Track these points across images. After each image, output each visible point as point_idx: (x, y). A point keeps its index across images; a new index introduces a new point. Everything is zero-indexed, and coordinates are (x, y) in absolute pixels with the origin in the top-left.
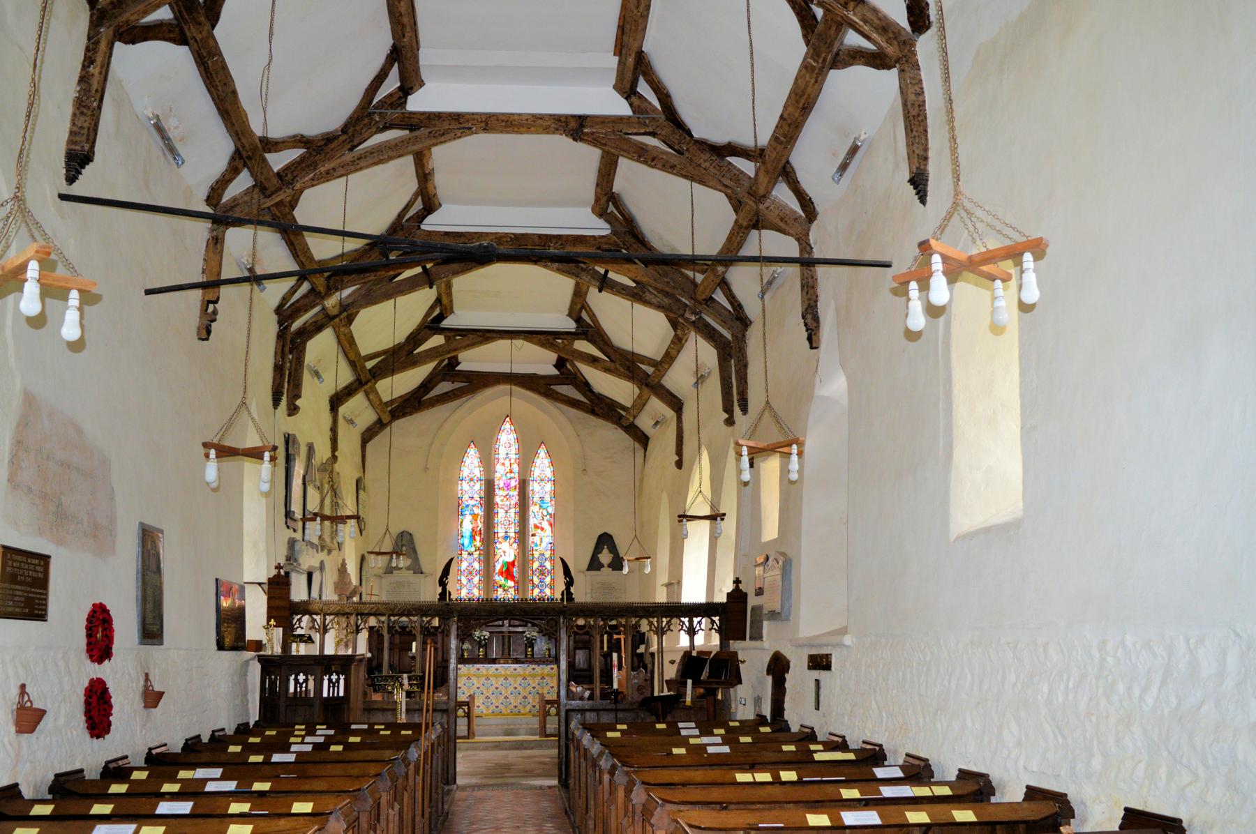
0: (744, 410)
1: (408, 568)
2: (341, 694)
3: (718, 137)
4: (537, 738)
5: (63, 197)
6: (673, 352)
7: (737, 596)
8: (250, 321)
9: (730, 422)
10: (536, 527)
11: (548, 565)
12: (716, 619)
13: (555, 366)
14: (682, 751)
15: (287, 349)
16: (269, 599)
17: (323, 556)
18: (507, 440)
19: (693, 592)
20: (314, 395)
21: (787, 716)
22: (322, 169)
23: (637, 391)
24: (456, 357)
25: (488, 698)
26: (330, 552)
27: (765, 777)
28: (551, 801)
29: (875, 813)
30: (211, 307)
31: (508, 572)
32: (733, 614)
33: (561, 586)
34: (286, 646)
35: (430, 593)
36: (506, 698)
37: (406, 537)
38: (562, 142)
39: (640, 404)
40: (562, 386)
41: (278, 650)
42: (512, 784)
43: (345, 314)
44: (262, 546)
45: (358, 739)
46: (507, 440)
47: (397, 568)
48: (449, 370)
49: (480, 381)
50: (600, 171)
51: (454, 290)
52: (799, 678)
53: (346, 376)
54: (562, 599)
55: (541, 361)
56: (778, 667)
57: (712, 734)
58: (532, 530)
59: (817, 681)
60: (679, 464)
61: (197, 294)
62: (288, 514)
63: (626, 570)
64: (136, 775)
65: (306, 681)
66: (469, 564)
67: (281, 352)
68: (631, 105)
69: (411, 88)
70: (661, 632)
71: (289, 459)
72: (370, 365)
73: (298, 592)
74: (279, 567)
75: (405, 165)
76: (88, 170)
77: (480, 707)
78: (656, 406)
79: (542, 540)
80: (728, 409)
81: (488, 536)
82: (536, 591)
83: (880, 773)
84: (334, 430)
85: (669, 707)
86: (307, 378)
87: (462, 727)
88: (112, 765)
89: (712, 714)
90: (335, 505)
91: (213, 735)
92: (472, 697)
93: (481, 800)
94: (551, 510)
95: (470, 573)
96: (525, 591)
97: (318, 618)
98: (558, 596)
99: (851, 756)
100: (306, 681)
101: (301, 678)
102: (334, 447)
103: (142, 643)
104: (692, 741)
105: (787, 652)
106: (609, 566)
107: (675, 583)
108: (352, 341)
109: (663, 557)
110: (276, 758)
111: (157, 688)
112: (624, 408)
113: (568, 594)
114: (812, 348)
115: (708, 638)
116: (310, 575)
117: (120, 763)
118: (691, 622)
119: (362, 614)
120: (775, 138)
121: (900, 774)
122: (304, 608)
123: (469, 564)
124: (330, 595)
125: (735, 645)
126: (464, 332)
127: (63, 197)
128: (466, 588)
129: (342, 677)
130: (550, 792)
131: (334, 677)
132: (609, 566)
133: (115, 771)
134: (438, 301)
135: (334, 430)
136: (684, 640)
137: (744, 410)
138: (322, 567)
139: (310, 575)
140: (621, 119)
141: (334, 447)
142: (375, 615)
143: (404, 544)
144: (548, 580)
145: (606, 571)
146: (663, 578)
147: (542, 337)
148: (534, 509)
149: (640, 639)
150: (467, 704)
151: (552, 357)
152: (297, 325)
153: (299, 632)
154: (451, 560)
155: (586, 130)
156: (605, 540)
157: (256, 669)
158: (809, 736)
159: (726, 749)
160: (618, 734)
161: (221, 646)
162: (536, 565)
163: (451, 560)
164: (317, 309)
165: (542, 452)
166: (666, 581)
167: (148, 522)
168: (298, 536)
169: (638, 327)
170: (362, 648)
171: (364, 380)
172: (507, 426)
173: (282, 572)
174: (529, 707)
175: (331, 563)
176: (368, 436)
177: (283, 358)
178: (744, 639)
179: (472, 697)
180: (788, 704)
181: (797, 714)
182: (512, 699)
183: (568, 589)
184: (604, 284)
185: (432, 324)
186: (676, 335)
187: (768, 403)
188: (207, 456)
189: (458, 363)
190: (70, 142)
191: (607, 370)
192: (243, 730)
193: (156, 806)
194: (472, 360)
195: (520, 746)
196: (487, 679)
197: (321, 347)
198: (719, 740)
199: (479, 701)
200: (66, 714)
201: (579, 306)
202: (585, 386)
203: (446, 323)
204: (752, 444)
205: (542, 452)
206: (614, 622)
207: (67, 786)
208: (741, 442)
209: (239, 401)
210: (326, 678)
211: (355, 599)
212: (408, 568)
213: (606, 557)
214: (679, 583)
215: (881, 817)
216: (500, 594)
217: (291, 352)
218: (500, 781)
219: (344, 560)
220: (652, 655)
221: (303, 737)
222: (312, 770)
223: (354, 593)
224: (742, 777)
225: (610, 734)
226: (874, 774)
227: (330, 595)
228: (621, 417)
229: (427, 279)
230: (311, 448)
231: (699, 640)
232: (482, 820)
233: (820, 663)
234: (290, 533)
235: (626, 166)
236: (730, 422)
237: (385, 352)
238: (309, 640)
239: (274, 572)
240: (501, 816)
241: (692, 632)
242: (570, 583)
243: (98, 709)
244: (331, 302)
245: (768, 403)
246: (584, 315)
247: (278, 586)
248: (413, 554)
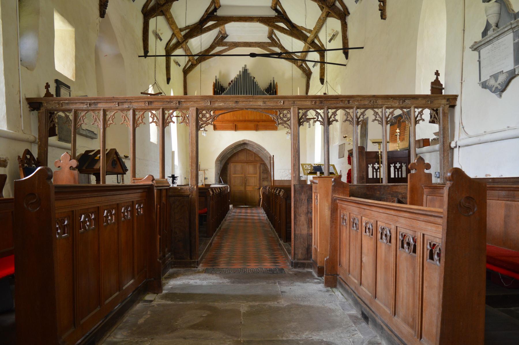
78: (314, 56)
131: (398, 165)
246: (278, 7)
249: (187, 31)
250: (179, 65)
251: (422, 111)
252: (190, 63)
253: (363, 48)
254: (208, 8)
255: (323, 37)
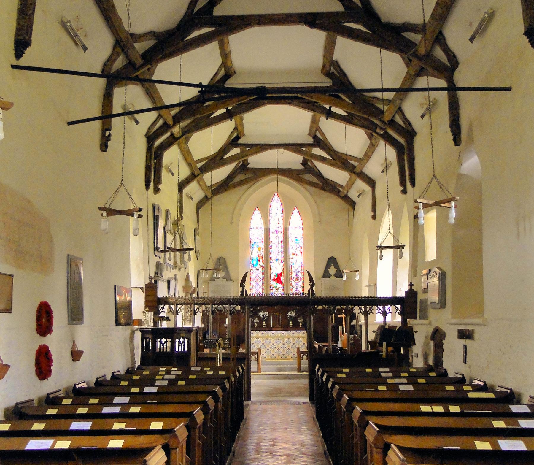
0: (413, 184)
1: (223, 278)
2: (186, 349)
3: (397, 19)
4: (296, 373)
5: (14, 67)
6: (370, 154)
7: (412, 294)
8: (131, 140)
9: (404, 192)
10: (293, 254)
11: (300, 275)
12: (399, 306)
13: (302, 164)
14: (384, 388)
15: (153, 157)
16: (146, 296)
17: (176, 271)
18: (276, 207)
19: (384, 291)
20: (169, 183)
21: (445, 366)
22: (167, 52)
23: (349, 176)
24: (247, 160)
25: (268, 349)
26: (180, 269)
27: (439, 409)
28: (305, 412)
29: (521, 442)
30: (107, 133)
31: (278, 279)
32: (409, 304)
33: (308, 287)
34: (155, 323)
35: (234, 292)
36: (278, 350)
37: (222, 261)
38: (303, 29)
39: (350, 184)
40: (306, 175)
41: (151, 325)
42: (282, 401)
43: (184, 137)
44: (141, 266)
45: (194, 377)
46: (276, 207)
47: (216, 278)
48: (243, 168)
49: (260, 173)
50: (325, 48)
51: (244, 121)
52: (452, 345)
53: (184, 172)
54: (309, 294)
55: (292, 160)
56: (438, 336)
57: (400, 377)
58: (291, 256)
59: (465, 347)
60: (374, 217)
61: (98, 124)
62: (156, 249)
63: (345, 278)
64: (66, 401)
65: (166, 342)
66: (257, 274)
67: (148, 159)
68: (343, 5)
69: (216, 2)
70: (366, 314)
71: (156, 219)
72: (199, 165)
73: (162, 292)
74: (151, 278)
75: (213, 47)
76: (28, 52)
77: (264, 354)
78: (360, 184)
79: (297, 262)
80: (403, 183)
81: (267, 259)
82: (294, 290)
83: (515, 409)
84: (180, 202)
85: (373, 359)
86: (164, 173)
87: (253, 367)
88: (51, 396)
89: (400, 363)
90: (182, 244)
91: (113, 375)
92: (259, 349)
93: (264, 411)
94: (302, 245)
95: (258, 280)
96: (287, 290)
97: (173, 306)
98: (306, 292)
99: (492, 396)
100: (166, 342)
101: (163, 340)
102: (181, 211)
103: (69, 324)
104: (389, 381)
105: (444, 327)
106: (335, 275)
107: (373, 285)
108: (189, 152)
109: (366, 271)
110: (147, 390)
111: (80, 349)
112: (342, 187)
113: (311, 291)
114: (456, 145)
115: (394, 317)
116: (169, 283)
117: (57, 394)
118: (384, 308)
119: (197, 304)
120: (433, 16)
121: (527, 410)
122: (165, 301)
123: (257, 274)
124: (180, 293)
125: (411, 322)
126: (251, 146)
127: (14, 67)
128: (255, 288)
129: (186, 340)
130: (304, 406)
131: (182, 340)
132: (335, 275)
133: (52, 400)
134: (236, 128)
135: (180, 202)
136: (380, 319)
137: (413, 184)
138: (175, 278)
139: (169, 283)
140: (337, 14)
141: (181, 211)
142: (204, 304)
143: (221, 264)
144: (300, 283)
145: (333, 278)
146: (366, 282)
147: (294, 147)
148: (292, 244)
149: (353, 317)
150: (257, 353)
151: (299, 158)
152: (158, 143)
153: (162, 314)
154: (247, 273)
155: (317, 22)
156: (332, 261)
157: (138, 336)
158: (460, 381)
159: (411, 388)
160: (344, 375)
161: (118, 323)
162: (293, 275)
163: (247, 273)
164: (168, 134)
165: (296, 211)
166: (368, 284)
167: (71, 253)
168: (161, 261)
169: (350, 139)
170: (198, 322)
171: (196, 175)
172: (276, 198)
173: (153, 281)
174: (291, 355)
175: (181, 275)
176: (200, 205)
177: (151, 162)
178: (416, 318)
179: (259, 349)
180: (445, 359)
181: (452, 365)
182: (281, 350)
183: (312, 288)
184: (329, 114)
185: (233, 142)
186: (371, 143)
187: (434, 176)
188: (102, 215)
189: (248, 164)
190: (17, 35)
191: (332, 165)
192: (130, 372)
193: (70, 424)
194: (257, 160)
195: (287, 377)
196: (268, 339)
197: (171, 156)
198: (405, 381)
199: (263, 352)
200: (23, 364)
201: (314, 129)
202: (319, 175)
203: (240, 141)
204: (425, 201)
205: (296, 211)
206: (339, 307)
207: (23, 410)
208: (419, 200)
209: (119, 184)
210: (177, 340)
211: (195, 295)
212: (223, 278)
213: (332, 270)
214: (375, 285)
215: (526, 445)
216: (274, 292)
217: (155, 159)
218: (275, 399)
219: (188, 274)
220: (361, 326)
221: (163, 375)
222: (166, 398)
223: (193, 292)
224: (425, 409)
225: (339, 375)
226: (510, 409)
227: (180, 293)
228: (340, 191)
229: (229, 115)
230: (167, 212)
231: (389, 318)
232: (265, 423)
233: (465, 335)
234: (157, 259)
235: (342, 42)
236: (404, 192)
237: (207, 158)
238: (168, 319)
239: (148, 281)
240: (276, 421)
241: (384, 314)
242: (312, 285)
243: (43, 364)
244: (176, 130)
245: (434, 176)
246: (318, 134)
247: (150, 289)
248: (226, 269)
249: (182, 108)
250: (192, 199)
251: (353, 307)
252: (160, 122)
253: (508, 89)
254: (214, 76)
255: (373, 168)
